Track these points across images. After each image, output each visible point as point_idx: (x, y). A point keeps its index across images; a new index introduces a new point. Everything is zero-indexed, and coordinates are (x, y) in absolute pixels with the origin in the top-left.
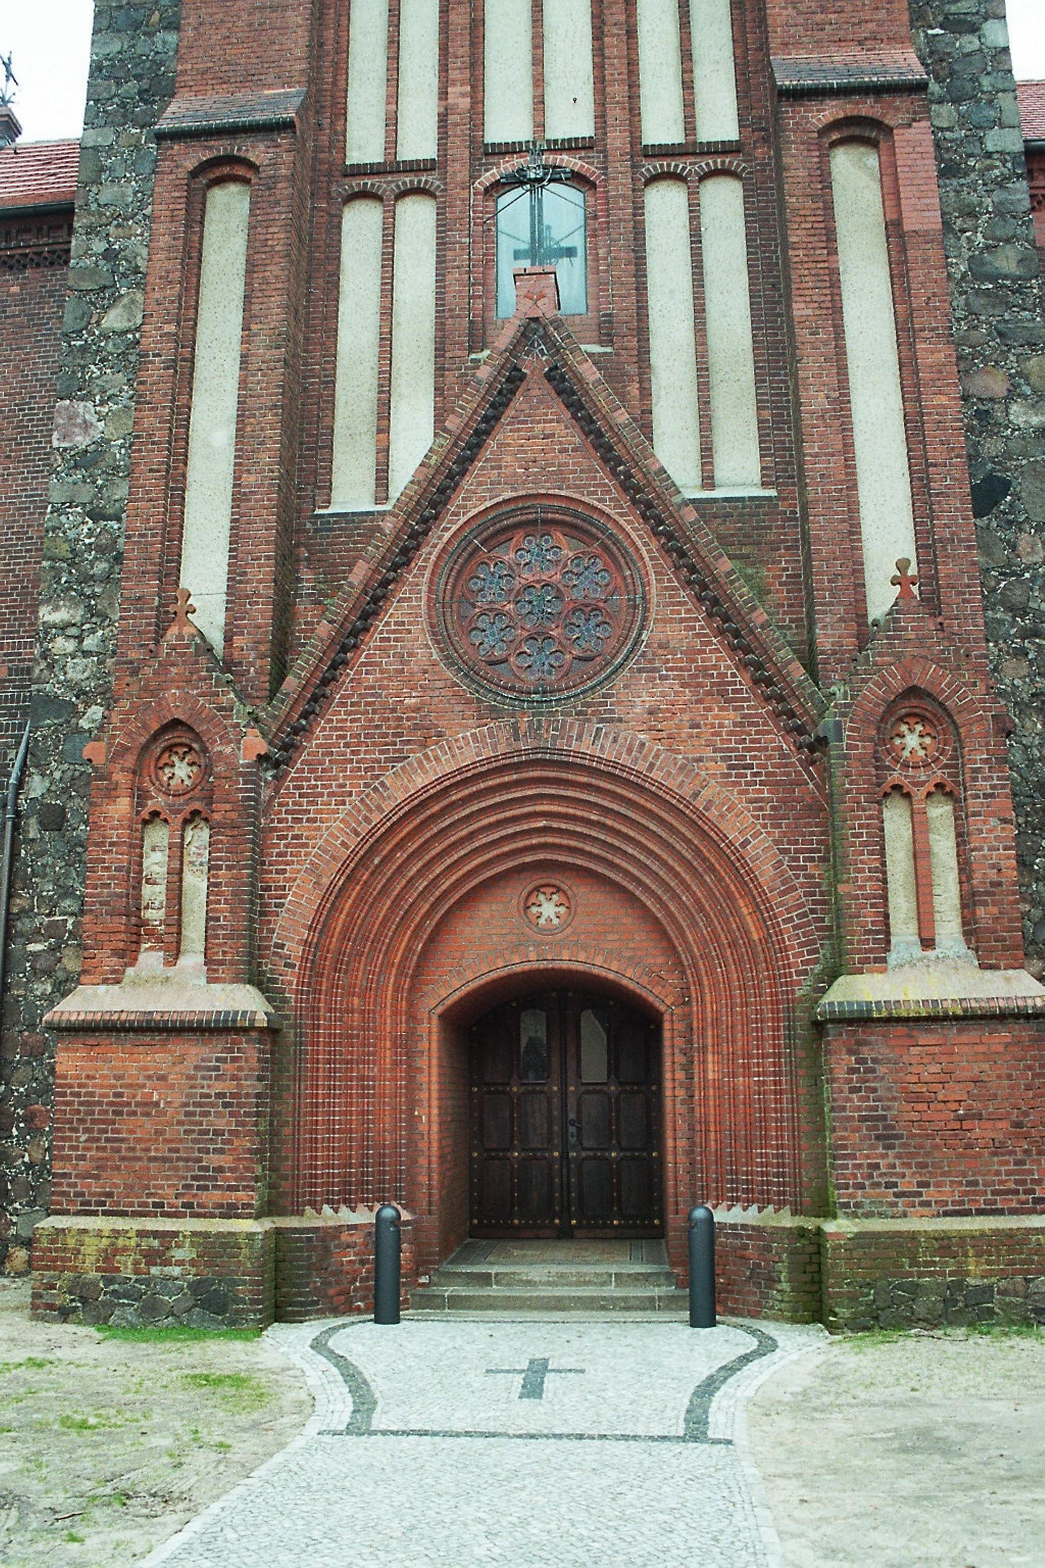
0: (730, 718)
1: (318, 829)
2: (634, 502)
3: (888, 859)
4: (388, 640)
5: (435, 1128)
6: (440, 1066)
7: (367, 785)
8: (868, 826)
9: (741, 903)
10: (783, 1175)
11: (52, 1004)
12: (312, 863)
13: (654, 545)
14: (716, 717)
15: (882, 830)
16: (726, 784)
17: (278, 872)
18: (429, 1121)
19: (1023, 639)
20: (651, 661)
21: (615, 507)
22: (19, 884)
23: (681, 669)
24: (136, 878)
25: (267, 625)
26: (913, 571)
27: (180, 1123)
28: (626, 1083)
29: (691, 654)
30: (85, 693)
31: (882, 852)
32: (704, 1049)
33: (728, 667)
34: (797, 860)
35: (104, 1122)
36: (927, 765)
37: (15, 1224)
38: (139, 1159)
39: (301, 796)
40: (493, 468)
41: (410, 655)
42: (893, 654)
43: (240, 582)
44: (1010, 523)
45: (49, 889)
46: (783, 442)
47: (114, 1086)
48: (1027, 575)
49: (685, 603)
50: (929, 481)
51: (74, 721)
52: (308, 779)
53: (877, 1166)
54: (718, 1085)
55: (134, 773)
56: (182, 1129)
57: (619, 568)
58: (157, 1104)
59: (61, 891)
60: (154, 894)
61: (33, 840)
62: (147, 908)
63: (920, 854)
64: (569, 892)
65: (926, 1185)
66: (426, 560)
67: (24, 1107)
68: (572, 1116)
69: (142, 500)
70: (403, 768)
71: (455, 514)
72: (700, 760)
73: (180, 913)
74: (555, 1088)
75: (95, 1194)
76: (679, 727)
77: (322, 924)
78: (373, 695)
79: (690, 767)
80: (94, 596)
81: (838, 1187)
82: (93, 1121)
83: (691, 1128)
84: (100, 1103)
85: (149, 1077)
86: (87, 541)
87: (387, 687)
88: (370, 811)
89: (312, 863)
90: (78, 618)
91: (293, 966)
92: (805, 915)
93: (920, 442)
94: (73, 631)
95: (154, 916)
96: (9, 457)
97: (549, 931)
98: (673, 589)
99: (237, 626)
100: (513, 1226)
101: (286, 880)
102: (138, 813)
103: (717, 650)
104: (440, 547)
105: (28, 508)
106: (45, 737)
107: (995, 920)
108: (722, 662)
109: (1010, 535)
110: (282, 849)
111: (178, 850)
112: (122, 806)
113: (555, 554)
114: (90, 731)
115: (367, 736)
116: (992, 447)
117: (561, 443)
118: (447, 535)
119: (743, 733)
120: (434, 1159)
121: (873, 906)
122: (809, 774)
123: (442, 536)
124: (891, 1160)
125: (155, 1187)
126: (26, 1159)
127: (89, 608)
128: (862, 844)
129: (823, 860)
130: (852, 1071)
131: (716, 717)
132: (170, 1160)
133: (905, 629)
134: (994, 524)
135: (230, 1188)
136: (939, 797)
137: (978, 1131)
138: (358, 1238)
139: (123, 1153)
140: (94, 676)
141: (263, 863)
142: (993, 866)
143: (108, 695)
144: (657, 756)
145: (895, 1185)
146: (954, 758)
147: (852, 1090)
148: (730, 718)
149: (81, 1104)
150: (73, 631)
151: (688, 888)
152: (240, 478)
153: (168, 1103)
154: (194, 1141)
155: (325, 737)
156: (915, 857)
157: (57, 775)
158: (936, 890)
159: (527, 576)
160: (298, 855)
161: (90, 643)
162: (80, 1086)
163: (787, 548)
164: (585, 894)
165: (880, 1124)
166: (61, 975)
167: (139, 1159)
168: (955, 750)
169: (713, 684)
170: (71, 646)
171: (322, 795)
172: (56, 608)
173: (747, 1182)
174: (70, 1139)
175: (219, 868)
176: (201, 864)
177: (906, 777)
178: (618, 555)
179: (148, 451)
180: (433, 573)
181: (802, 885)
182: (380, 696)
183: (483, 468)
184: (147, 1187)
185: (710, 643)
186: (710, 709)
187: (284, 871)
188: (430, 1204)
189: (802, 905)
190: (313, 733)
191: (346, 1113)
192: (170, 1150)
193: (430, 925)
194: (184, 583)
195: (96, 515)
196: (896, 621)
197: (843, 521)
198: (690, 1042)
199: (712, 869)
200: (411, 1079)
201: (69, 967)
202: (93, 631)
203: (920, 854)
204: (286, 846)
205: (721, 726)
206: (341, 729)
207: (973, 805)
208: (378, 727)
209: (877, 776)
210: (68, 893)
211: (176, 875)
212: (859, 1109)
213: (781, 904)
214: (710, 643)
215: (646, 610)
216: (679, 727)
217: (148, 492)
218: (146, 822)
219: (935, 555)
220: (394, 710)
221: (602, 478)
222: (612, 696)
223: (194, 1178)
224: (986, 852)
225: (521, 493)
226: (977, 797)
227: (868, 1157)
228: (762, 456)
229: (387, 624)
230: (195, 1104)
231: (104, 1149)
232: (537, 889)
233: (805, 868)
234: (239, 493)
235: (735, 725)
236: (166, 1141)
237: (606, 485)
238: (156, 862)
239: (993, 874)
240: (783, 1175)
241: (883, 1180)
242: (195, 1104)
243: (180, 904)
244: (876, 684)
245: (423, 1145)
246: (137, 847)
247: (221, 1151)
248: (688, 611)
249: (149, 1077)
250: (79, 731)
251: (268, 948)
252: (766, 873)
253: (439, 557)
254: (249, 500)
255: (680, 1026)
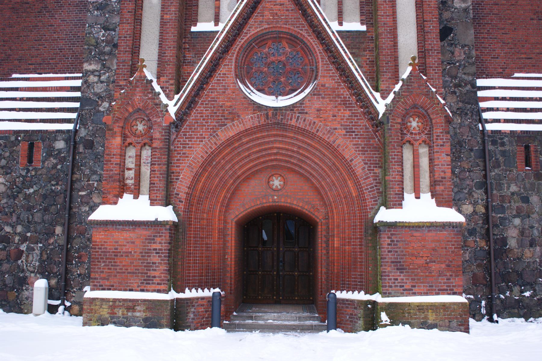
0: (347, 113)
1: (192, 151)
2: (314, 31)
3: (404, 168)
4: (220, 80)
5: (233, 263)
6: (235, 240)
7: (211, 135)
8: (397, 155)
9: (349, 182)
10: (362, 282)
11: (89, 215)
12: (190, 164)
13: (321, 48)
14: (342, 113)
15: (402, 157)
16: (345, 138)
17: (177, 166)
18: (231, 260)
19: (455, 88)
20: (319, 91)
21: (307, 33)
22: (76, 170)
23: (330, 95)
24: (123, 167)
25: (173, 73)
26: (416, 61)
27: (139, 259)
28: (301, 248)
29: (333, 89)
30: (102, 97)
31: (402, 165)
32: (333, 236)
33: (347, 95)
34: (370, 167)
35: (110, 259)
36: (419, 134)
37: (74, 296)
38: (124, 273)
39: (186, 138)
40: (261, 16)
41: (228, 86)
42: (409, 92)
43: (164, 56)
44: (452, 44)
45: (87, 172)
46: (369, 10)
47: (114, 246)
48: (457, 64)
49: (331, 70)
50: (424, 27)
51: (97, 108)
52: (189, 132)
53: (397, 279)
54: (338, 249)
55: (122, 127)
56: (140, 261)
57: (307, 56)
58: (131, 252)
59: (92, 172)
60: (130, 174)
61: (81, 153)
62: (127, 179)
63: (416, 166)
64: (285, 177)
65: (414, 286)
66: (235, 50)
67: (77, 253)
68: (281, 259)
69: (125, 23)
70: (225, 129)
71: (245, 33)
72: (336, 129)
73: (139, 181)
74: (275, 249)
75: (107, 286)
76: (328, 116)
77: (193, 186)
78: (213, 101)
79: (332, 131)
80: (105, 60)
81: (383, 287)
82: (107, 259)
83: (328, 264)
84: (109, 252)
85: (128, 242)
86: (102, 39)
87: (219, 98)
88: (212, 144)
89: (190, 164)
90: (99, 69)
91: (182, 202)
92: (373, 187)
93: (421, 12)
94: (97, 73)
95: (130, 182)
96: (70, 4)
97: (276, 190)
98: (328, 64)
99: (162, 73)
100: (295, 299)
101: (180, 169)
102: (124, 143)
103: (343, 88)
104: (240, 45)
105: (78, 25)
106: (86, 114)
107: (443, 191)
108: (346, 93)
109: (451, 49)
110: (179, 158)
111: (139, 157)
112: (118, 140)
113: (283, 50)
114: (103, 112)
115: (211, 116)
116: (447, 15)
117: (287, 7)
118: (243, 41)
119: (352, 119)
120: (233, 274)
121: (398, 185)
122: (376, 135)
123: (241, 41)
124: (402, 277)
125: (130, 283)
126: (79, 272)
127: (104, 66)
128: (395, 162)
129: (380, 167)
130: (389, 244)
131: (342, 113)
132: (136, 273)
133: (413, 82)
134: (446, 44)
135: (158, 284)
136: (423, 145)
137: (434, 267)
138: (205, 302)
139: (118, 270)
140: (105, 91)
141: (171, 163)
142: (443, 171)
143: (111, 98)
144: (320, 127)
145: (403, 286)
146: (430, 131)
147: (389, 252)
148: (347, 113)
149: (102, 252)
150: (97, 73)
151: (329, 176)
152: (163, 16)
153: (135, 252)
154: (145, 266)
155: (195, 116)
156: (414, 167)
157: (91, 128)
158: (421, 180)
159: (272, 58)
160: (184, 160)
161: (103, 78)
162: (102, 245)
163: (369, 51)
164: (291, 177)
165: (399, 264)
166: (92, 204)
167: (124, 273)
168: (430, 128)
169: (341, 101)
170: (96, 79)
171: (194, 138)
172: (90, 64)
173: (348, 284)
174: (98, 265)
175: (155, 164)
176: (148, 163)
177: (412, 138)
178: (307, 51)
179: (127, 4)
180: (237, 55)
181: (372, 176)
182: (216, 101)
183: (257, 16)
184: (127, 283)
185: (340, 85)
186: (340, 110)
187: (179, 166)
188: (231, 290)
189: (372, 184)
190: (190, 115)
191: (201, 257)
192: (136, 270)
193: (233, 188)
194: (141, 57)
195: (106, 29)
196: (411, 79)
197: (392, 41)
198: (328, 233)
199: (338, 169)
200: (225, 244)
201: (95, 201)
202: (104, 74)
203: (416, 166)
204: (180, 157)
205: (344, 116)
206: (202, 113)
207: (436, 149)
208: (215, 113)
209: (401, 137)
210: (95, 173)
211: (138, 166)
212: (391, 258)
213: (365, 183)
214: (340, 85)
215: (317, 72)
216: (328, 116)
217: (127, 20)
218: (126, 147)
219: (425, 56)
220: (221, 107)
221: (302, 21)
222: (303, 104)
223: (144, 280)
224: (440, 166)
225: (271, 26)
226: (438, 145)
227: (393, 276)
228: (361, 15)
229: (220, 74)
230: (145, 253)
231: (110, 269)
232: (273, 175)
233: (373, 170)
234: (163, 22)
235: (349, 116)
236: (134, 266)
237: (303, 24)
238: (130, 163)
239: (442, 175)
240: (362, 282)
241: (399, 285)
242: (145, 253)
243: (140, 178)
244: (402, 103)
245: (228, 269)
246: (123, 156)
247: (155, 270)
248: (333, 73)
249: (128, 242)
250: (99, 111)
251: (173, 195)
252: (359, 171)
253: (240, 49)
254: (167, 25)
255: (324, 227)
